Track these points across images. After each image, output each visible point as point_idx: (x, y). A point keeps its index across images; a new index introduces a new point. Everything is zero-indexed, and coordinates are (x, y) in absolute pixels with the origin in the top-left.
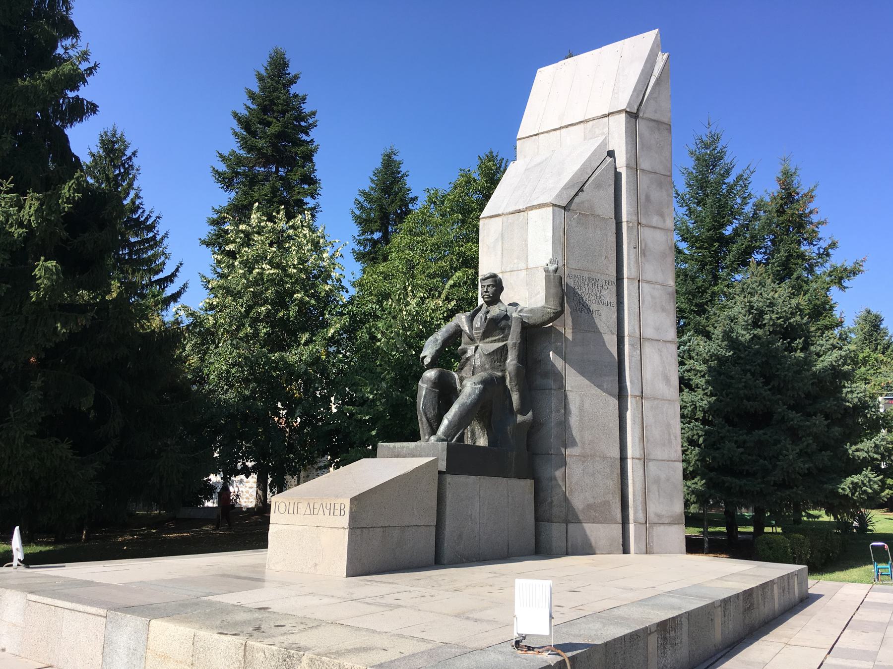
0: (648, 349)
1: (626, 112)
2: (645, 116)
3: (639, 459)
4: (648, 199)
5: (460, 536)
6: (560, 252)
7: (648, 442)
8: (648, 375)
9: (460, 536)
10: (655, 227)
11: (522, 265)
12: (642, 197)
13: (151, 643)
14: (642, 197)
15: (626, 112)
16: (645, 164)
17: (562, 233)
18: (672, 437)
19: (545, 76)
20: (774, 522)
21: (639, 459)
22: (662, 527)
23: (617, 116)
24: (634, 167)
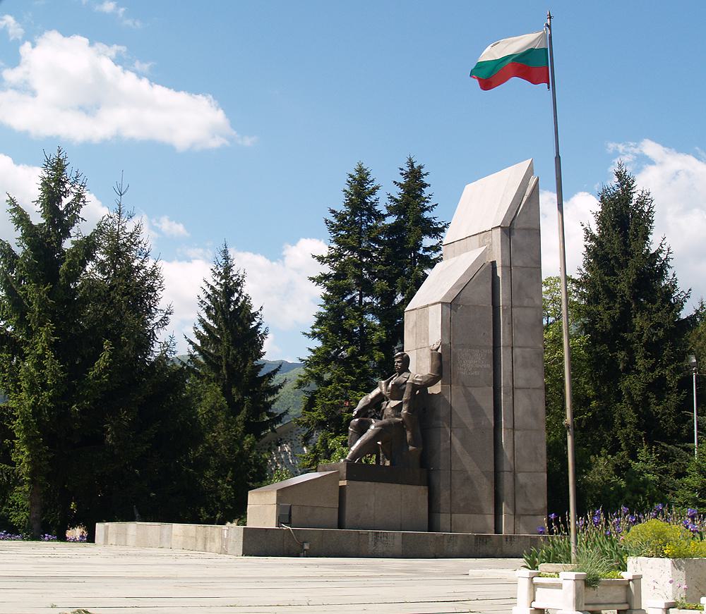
0: (518, 394)
1: (501, 227)
2: (518, 227)
3: (510, 472)
4: (520, 287)
5: (358, 516)
6: (447, 334)
7: (517, 460)
8: (518, 413)
9: (358, 516)
10: (526, 307)
11: (426, 344)
12: (515, 288)
13: (173, 532)
14: (515, 288)
15: (501, 227)
16: (518, 262)
17: (448, 321)
18: (539, 456)
19: (469, 189)
20: (7, 441)
21: (510, 472)
22: (528, 517)
23: (496, 230)
24: (509, 267)
